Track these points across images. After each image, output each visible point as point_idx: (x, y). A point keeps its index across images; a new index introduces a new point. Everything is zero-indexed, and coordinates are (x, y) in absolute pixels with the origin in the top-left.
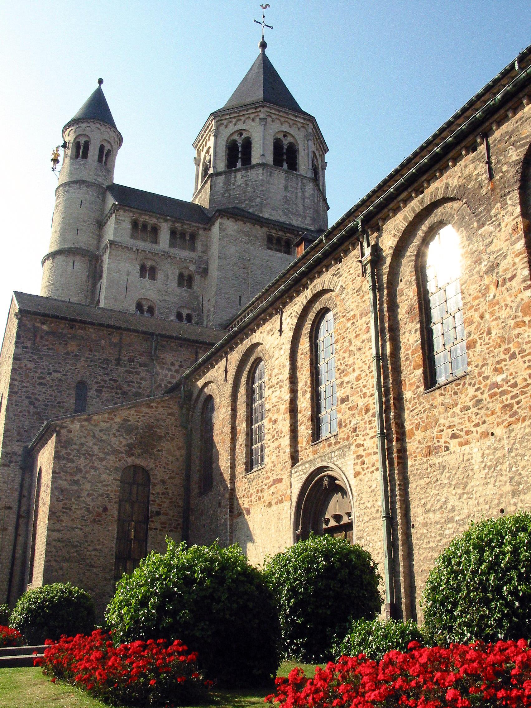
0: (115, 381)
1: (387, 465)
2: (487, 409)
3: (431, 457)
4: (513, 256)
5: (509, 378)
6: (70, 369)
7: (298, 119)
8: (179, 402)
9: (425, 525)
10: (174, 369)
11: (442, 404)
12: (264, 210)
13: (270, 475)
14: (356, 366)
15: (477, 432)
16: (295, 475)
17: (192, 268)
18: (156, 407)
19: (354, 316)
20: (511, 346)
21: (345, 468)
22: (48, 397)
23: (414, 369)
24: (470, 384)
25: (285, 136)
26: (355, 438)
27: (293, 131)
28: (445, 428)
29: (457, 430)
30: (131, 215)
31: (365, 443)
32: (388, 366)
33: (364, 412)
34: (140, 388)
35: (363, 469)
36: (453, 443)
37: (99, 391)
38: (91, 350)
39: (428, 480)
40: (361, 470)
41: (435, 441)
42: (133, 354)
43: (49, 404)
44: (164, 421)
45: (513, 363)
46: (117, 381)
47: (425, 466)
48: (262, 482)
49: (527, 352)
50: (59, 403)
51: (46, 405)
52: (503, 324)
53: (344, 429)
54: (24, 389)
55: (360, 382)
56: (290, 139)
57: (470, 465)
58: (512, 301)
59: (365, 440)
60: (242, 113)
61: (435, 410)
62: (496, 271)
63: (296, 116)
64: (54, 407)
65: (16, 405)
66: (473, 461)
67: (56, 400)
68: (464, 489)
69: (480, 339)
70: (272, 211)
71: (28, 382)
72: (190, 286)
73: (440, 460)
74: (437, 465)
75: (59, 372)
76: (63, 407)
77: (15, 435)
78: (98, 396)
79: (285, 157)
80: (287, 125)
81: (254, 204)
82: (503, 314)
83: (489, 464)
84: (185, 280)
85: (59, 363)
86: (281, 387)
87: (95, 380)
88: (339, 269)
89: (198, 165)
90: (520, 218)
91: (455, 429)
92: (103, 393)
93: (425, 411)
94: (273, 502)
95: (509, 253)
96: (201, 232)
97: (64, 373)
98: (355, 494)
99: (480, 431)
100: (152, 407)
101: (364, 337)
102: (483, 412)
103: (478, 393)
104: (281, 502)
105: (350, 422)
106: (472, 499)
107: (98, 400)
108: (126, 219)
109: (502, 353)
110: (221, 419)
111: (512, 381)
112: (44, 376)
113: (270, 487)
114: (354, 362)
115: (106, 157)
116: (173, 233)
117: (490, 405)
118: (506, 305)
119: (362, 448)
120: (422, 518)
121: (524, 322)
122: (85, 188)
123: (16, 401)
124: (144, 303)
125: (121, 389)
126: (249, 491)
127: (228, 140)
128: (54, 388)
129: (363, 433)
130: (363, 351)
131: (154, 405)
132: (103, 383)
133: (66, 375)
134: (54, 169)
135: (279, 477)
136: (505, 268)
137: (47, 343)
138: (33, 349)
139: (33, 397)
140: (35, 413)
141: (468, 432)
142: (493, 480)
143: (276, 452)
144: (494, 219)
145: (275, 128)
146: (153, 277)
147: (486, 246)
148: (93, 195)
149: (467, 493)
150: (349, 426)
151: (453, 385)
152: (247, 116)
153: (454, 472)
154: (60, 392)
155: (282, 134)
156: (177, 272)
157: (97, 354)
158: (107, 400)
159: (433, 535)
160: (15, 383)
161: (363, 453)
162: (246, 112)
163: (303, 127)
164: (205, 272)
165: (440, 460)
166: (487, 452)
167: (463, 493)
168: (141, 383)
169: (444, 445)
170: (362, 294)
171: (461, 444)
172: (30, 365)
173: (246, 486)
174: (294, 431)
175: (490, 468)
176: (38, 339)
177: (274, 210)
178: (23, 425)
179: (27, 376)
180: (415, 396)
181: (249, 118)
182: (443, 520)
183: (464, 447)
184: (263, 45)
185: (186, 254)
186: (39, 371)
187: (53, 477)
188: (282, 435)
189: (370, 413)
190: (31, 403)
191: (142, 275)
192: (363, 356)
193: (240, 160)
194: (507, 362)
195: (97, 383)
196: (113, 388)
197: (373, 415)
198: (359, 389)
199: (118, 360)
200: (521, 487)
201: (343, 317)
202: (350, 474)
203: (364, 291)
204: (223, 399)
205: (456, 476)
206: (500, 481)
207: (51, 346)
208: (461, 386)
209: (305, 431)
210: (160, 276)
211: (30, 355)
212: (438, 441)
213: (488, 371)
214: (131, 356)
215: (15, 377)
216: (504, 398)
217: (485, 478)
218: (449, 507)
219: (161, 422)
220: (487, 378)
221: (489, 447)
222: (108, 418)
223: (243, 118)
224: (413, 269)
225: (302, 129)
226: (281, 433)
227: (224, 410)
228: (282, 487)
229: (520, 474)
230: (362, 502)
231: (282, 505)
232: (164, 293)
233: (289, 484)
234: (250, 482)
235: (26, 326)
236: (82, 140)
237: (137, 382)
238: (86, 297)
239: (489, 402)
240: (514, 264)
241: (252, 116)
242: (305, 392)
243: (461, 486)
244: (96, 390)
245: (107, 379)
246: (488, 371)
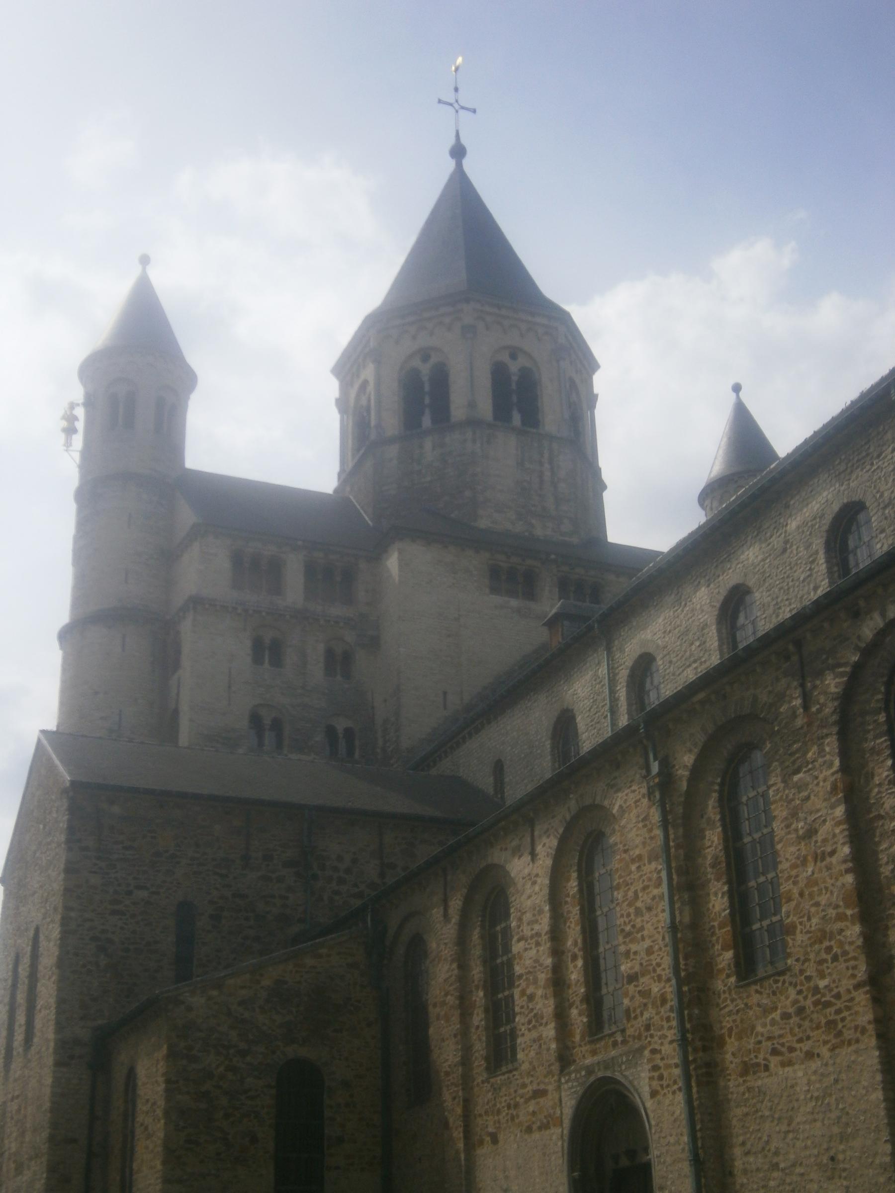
1: (693, 1084)
2: (811, 1021)
3: (748, 1078)
4: (832, 823)
5: (833, 985)
9: (745, 1172)
11: (759, 1005)
13: (527, 1080)
14: (646, 933)
15: (801, 1049)
16: (566, 1086)
19: (640, 857)
20: (833, 943)
21: (640, 1081)
23: (722, 949)
24: (791, 984)
25: (513, 356)
26: (649, 1039)
28: (763, 1039)
29: (778, 1043)
31: (663, 1048)
32: (689, 940)
33: (659, 1003)
35: (662, 1086)
36: (774, 1061)
39: (745, 1110)
40: (659, 1088)
41: (752, 1056)
45: (836, 967)
47: (742, 1089)
48: (515, 1091)
49: (850, 956)
52: (823, 913)
53: (634, 1022)
55: (652, 957)
56: (522, 361)
57: (794, 1094)
58: (833, 885)
59: (662, 1044)
61: (751, 1013)
62: (814, 839)
66: (798, 1089)
68: (789, 1125)
69: (801, 923)
73: (759, 1083)
74: (757, 1090)
82: (823, 899)
83: (816, 1094)
86: (538, 944)
88: (615, 778)
90: (839, 775)
91: (775, 1042)
93: (738, 1011)
94: (535, 1127)
95: (828, 819)
98: (653, 1123)
99: (804, 1049)
101: (656, 892)
102: (807, 1024)
103: (800, 998)
104: (544, 1127)
105: (642, 1014)
106: (798, 1139)
109: (823, 951)
111: (835, 991)
113: (527, 1101)
114: (643, 926)
117: (815, 1016)
118: (826, 888)
119: (658, 1056)
120: (741, 1162)
121: (846, 915)
126: (495, 1105)
129: (659, 1033)
130: (654, 912)
131: (324, 951)
135: (542, 1087)
136: (823, 837)
141: (791, 1050)
142: (821, 1116)
143: (535, 1046)
144: (810, 766)
147: (802, 800)
149: (793, 1131)
150: (640, 1019)
151: (771, 981)
153: (776, 1102)
156: (321, 647)
159: (755, 1187)
161: (661, 1064)
164: (373, 643)
165: (759, 1083)
166: (813, 1078)
167: (789, 1132)
169: (763, 1062)
170: (650, 826)
171: (783, 1065)
173: (490, 1095)
174: (561, 1016)
175: (817, 1098)
180: (726, 988)
182: (766, 1167)
183: (787, 1069)
184: (458, 152)
185: (337, 611)
187: (167, 1090)
188: (544, 1021)
189: (668, 1006)
191: (257, 659)
192: (655, 920)
193: (427, 411)
194: (829, 964)
197: (671, 1010)
198: (651, 968)
200: (849, 1130)
201: (626, 851)
202: (645, 1090)
203: (653, 821)
204: (442, 947)
205: (780, 1108)
206: (829, 1118)
208: (780, 984)
209: (578, 1017)
212: (756, 1057)
213: (811, 970)
216: (828, 1010)
217: (813, 1113)
218: (773, 1149)
220: (809, 979)
221: (815, 1072)
224: (717, 804)
226: (542, 1018)
227: (446, 967)
228: (546, 1102)
229: (848, 1113)
230: (663, 1135)
231: (547, 1132)
233: (557, 1101)
234: (495, 1089)
239: (813, 1012)
240: (834, 836)
242: (574, 958)
243: (786, 1122)
246: (811, 970)
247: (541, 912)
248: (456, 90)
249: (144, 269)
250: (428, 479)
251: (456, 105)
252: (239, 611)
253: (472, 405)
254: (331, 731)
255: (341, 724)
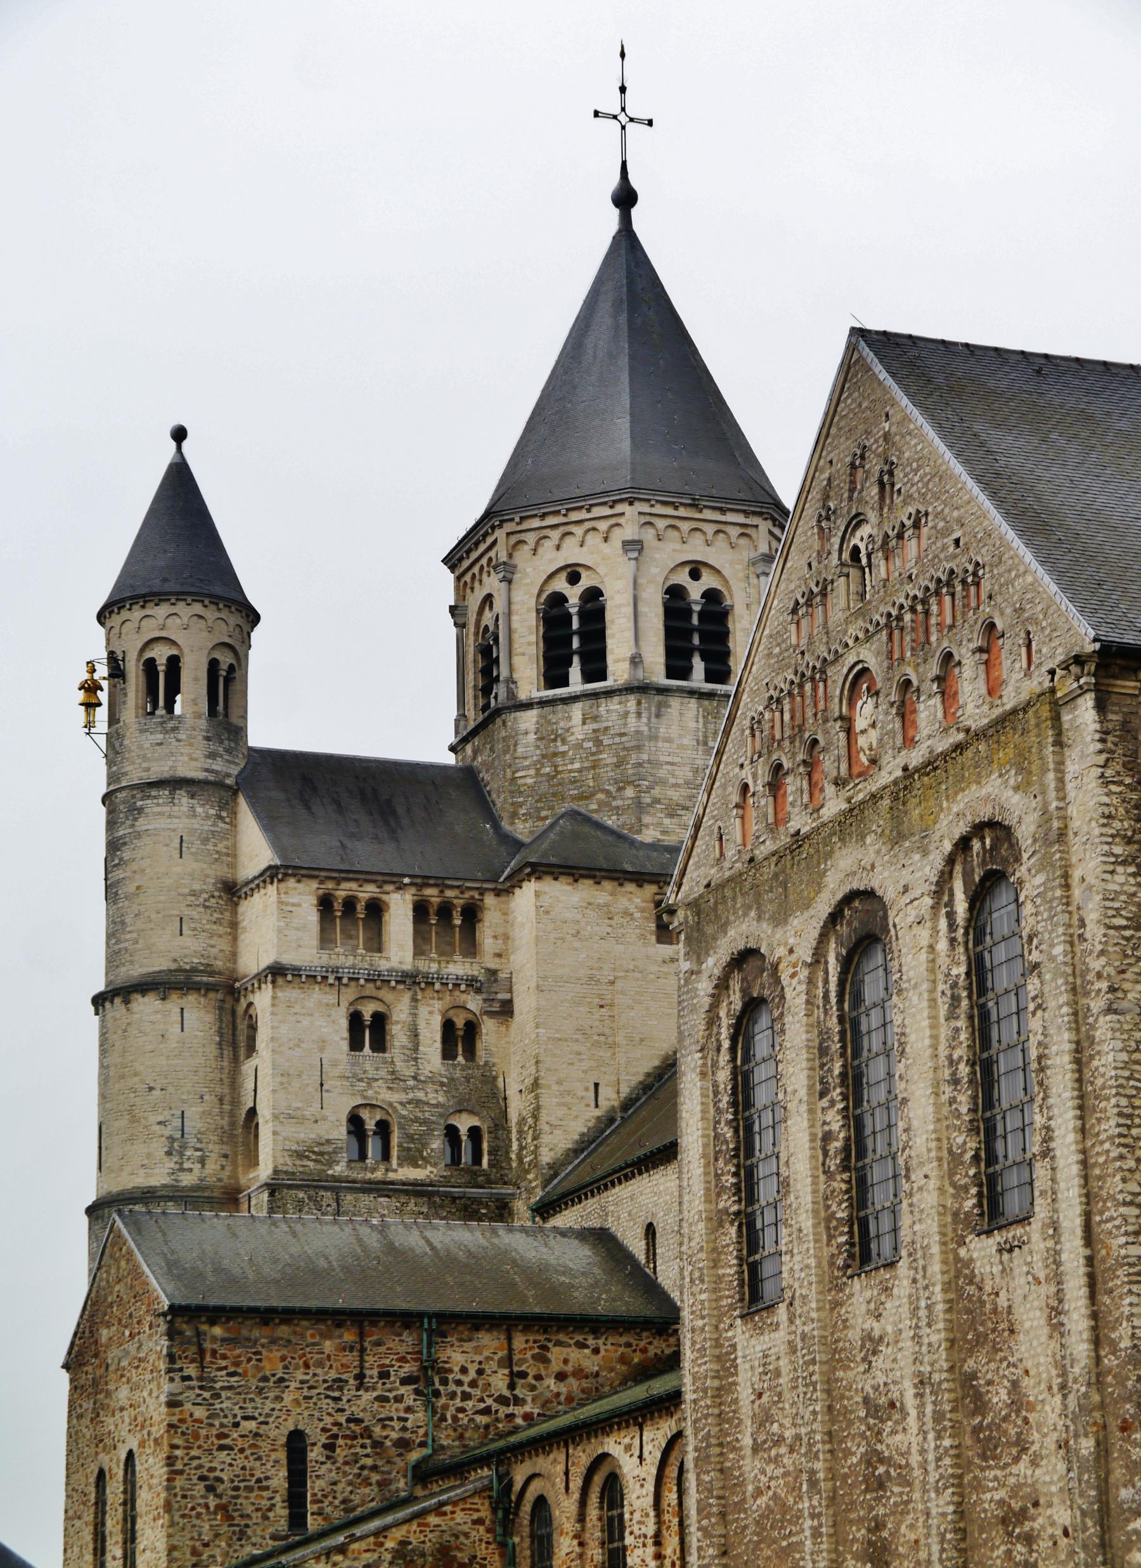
0: (358, 1421)
6: (273, 1410)
7: (731, 517)
8: (490, 1497)
10: (466, 1379)
12: (646, 819)
17: (474, 1003)
18: (453, 1512)
22: (238, 1471)
25: (695, 575)
27: (717, 555)
30: (314, 885)
34: (404, 1429)
37: (330, 1447)
38: (307, 1366)
42: (387, 1362)
43: (242, 1485)
44: (467, 1535)
46: (362, 1421)
50: (259, 1481)
51: (236, 1489)
54: (195, 1463)
56: (708, 581)
60: (574, 516)
63: (723, 511)
64: (250, 1489)
65: (184, 1497)
67: (252, 1475)
70: (667, 821)
71: (199, 1447)
72: (471, 1053)
75: (253, 1418)
76: (267, 1488)
77: (188, 1556)
78: (328, 1457)
79: (696, 640)
80: (698, 538)
81: (619, 803)
84: (460, 1038)
85: (252, 1400)
87: (321, 1425)
89: (460, 626)
92: (338, 1450)
96: (490, 900)
97: (261, 1419)
100: (445, 1514)
107: (328, 1465)
108: (303, 898)
110: (563, 1553)
112: (225, 1430)
115: (226, 683)
116: (420, 910)
122: (185, 800)
123: (182, 1489)
124: (365, 1114)
125: (370, 1437)
127: (541, 591)
128: (248, 1452)
131: (448, 1508)
132: (335, 1429)
133: (267, 1423)
134: (89, 725)
137: (223, 1363)
138: (201, 1379)
139: (212, 1475)
140: (217, 1507)
145: (666, 556)
146: (380, 1045)
148: (208, 817)
152: (588, 525)
154: (259, 1458)
155: (563, 576)
156: (437, 1021)
157: (319, 1371)
158: (346, 1463)
160: (178, 1453)
162: (583, 515)
163: (742, 534)
164: (506, 1010)
168: (406, 1420)
172: (200, 1413)
176: (208, 1358)
177: (671, 816)
178: (200, 1535)
179: (196, 1436)
181: (594, 529)
184: (625, 198)
185: (459, 968)
186: (217, 1423)
190: (210, 1489)
191: (356, 1044)
193: (576, 660)
195: (324, 1430)
196: (355, 1438)
199: (360, 1377)
207: (231, 1369)
210: (397, 1034)
211: (198, 1391)
214: (383, 1366)
215: (176, 1441)
219: (462, 1539)
222: (375, 1544)
223: (578, 531)
225: (743, 541)
232: (411, 1083)
235: (181, 1333)
236: (161, 654)
237: (399, 1419)
238: (221, 1100)
241: (603, 526)
244: (325, 1446)
245: (342, 1420)
247: (647, 1515)
248: (623, 89)
249: (179, 448)
250: (577, 765)
251: (623, 118)
252: (331, 981)
253: (636, 661)
254: (452, 1133)
255: (464, 1123)
